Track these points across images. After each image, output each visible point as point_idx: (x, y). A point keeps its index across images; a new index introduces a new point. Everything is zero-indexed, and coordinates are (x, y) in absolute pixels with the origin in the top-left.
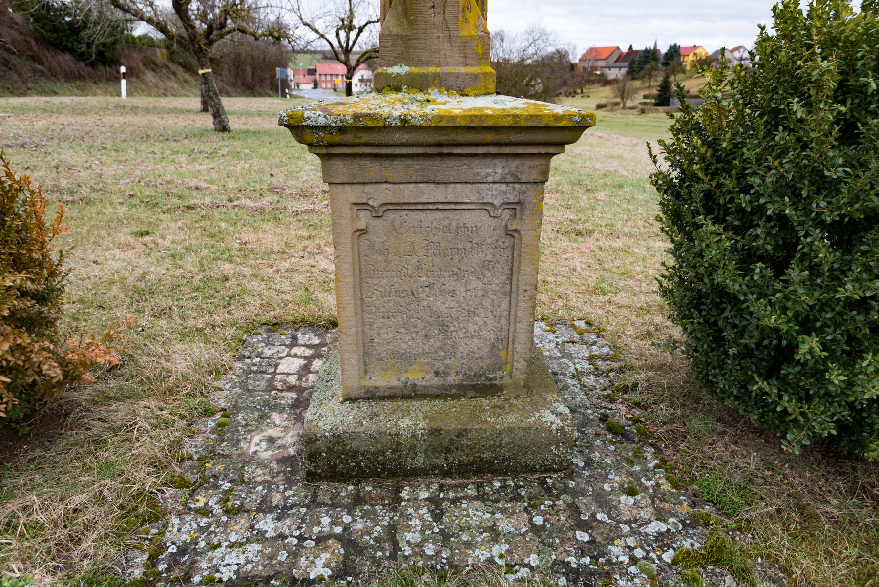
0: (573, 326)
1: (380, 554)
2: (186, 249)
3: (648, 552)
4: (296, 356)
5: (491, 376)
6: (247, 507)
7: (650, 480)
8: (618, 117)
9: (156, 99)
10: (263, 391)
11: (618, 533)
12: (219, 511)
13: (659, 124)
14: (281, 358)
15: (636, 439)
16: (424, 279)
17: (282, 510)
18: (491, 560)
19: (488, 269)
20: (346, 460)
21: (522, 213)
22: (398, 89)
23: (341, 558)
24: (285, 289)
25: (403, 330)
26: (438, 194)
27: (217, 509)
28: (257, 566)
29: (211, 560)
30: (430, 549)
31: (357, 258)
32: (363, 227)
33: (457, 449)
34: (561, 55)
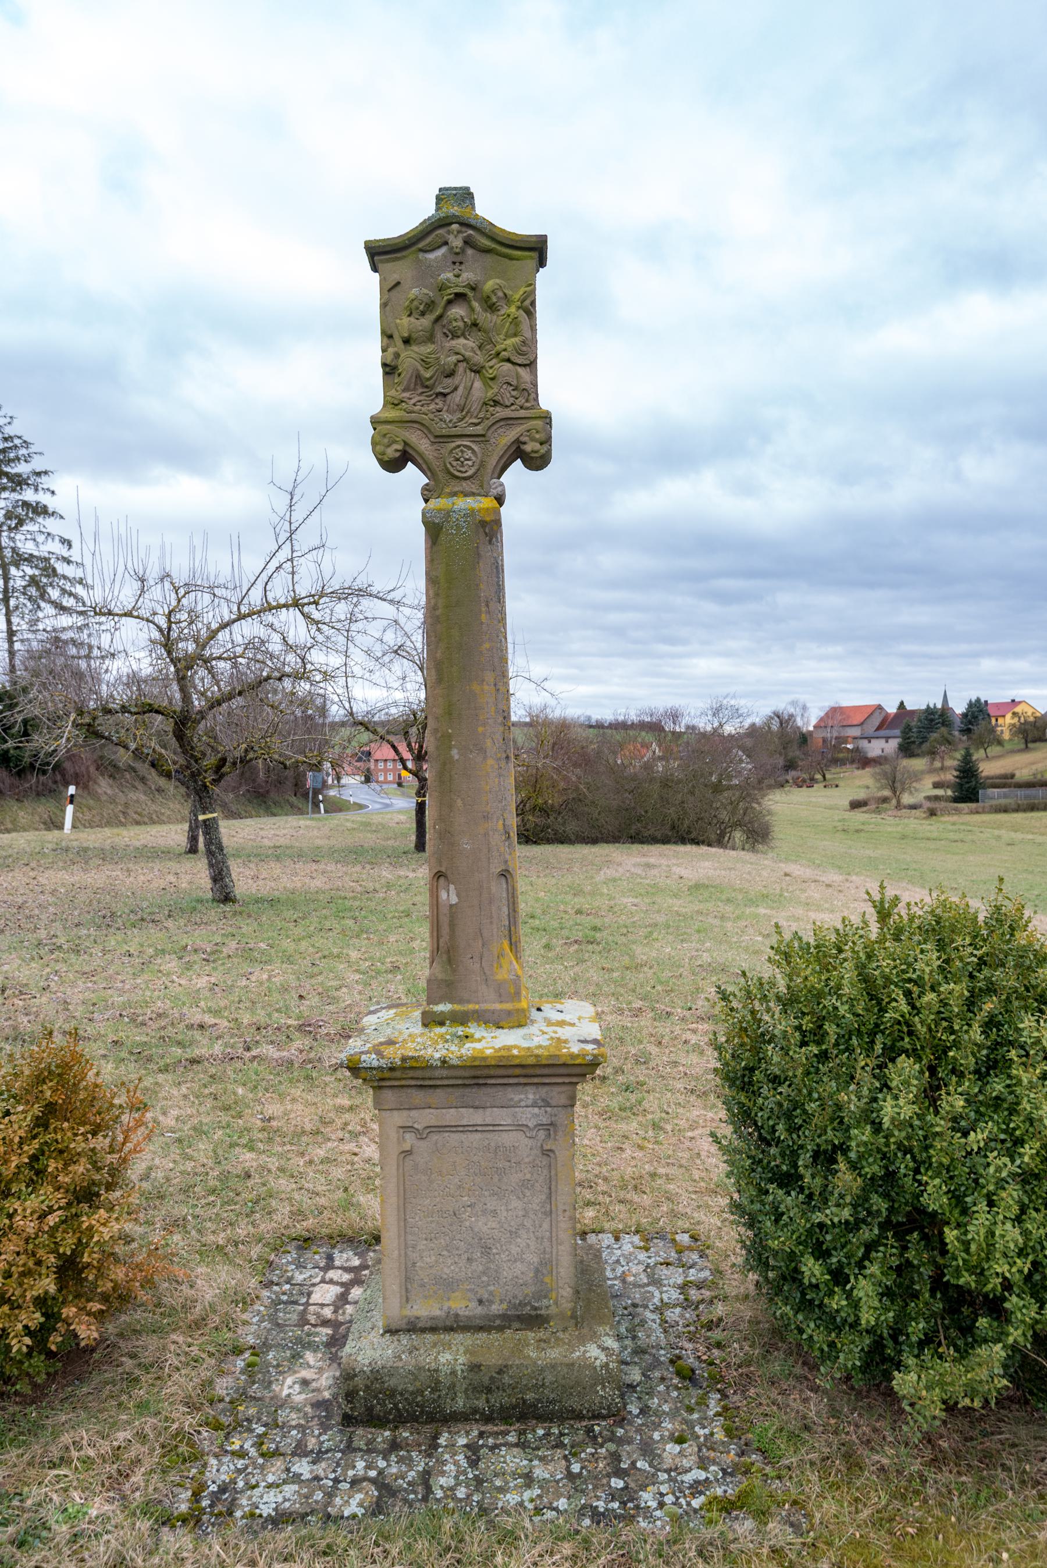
0: (674, 1241)
1: (412, 1496)
2: (194, 1129)
3: (677, 1498)
4: (331, 1282)
5: (536, 1305)
6: (282, 1450)
7: (704, 1427)
8: (889, 823)
9: (116, 831)
10: (295, 1326)
11: (654, 1480)
12: (256, 1454)
13: (961, 836)
14: (314, 1285)
15: (705, 1385)
16: (466, 1198)
17: (317, 1454)
18: (521, 1504)
19: (528, 1188)
20: (384, 1401)
21: (555, 1132)
22: (442, 1024)
23: (374, 1499)
24: (320, 1188)
25: (445, 1253)
26: (476, 1117)
27: (253, 1452)
28: (294, 1503)
29: (250, 1498)
30: (461, 1493)
31: (402, 1179)
32: (408, 1149)
33: (498, 1388)
34: (784, 721)
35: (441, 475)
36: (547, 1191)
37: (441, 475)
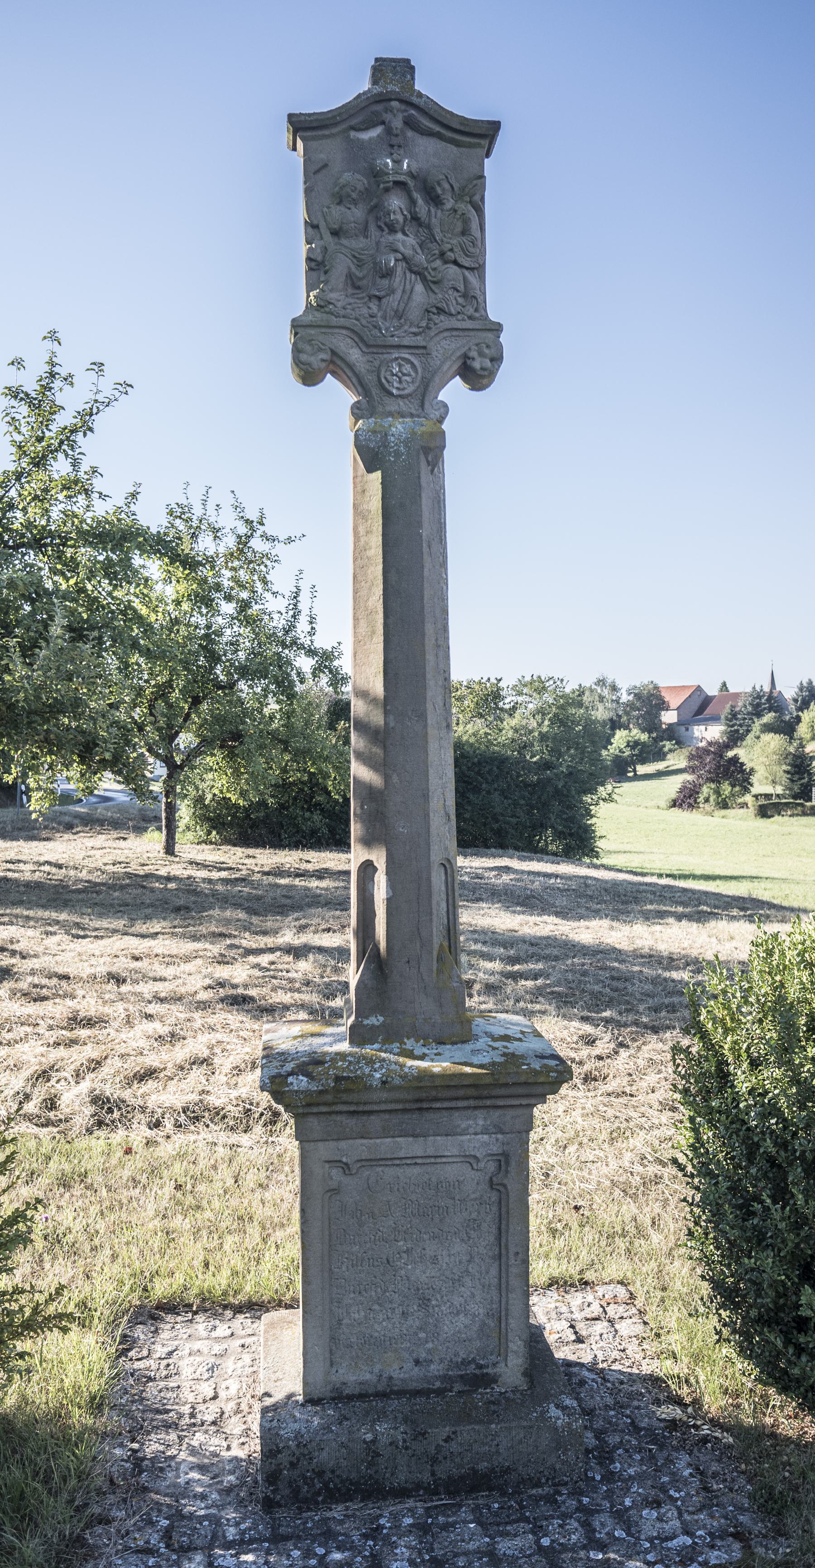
5: (482, 1362)
16: (401, 1243)
20: (312, 1479)
25: (376, 1307)
35: (375, 391)
36: (494, 1230)
37: (375, 391)
